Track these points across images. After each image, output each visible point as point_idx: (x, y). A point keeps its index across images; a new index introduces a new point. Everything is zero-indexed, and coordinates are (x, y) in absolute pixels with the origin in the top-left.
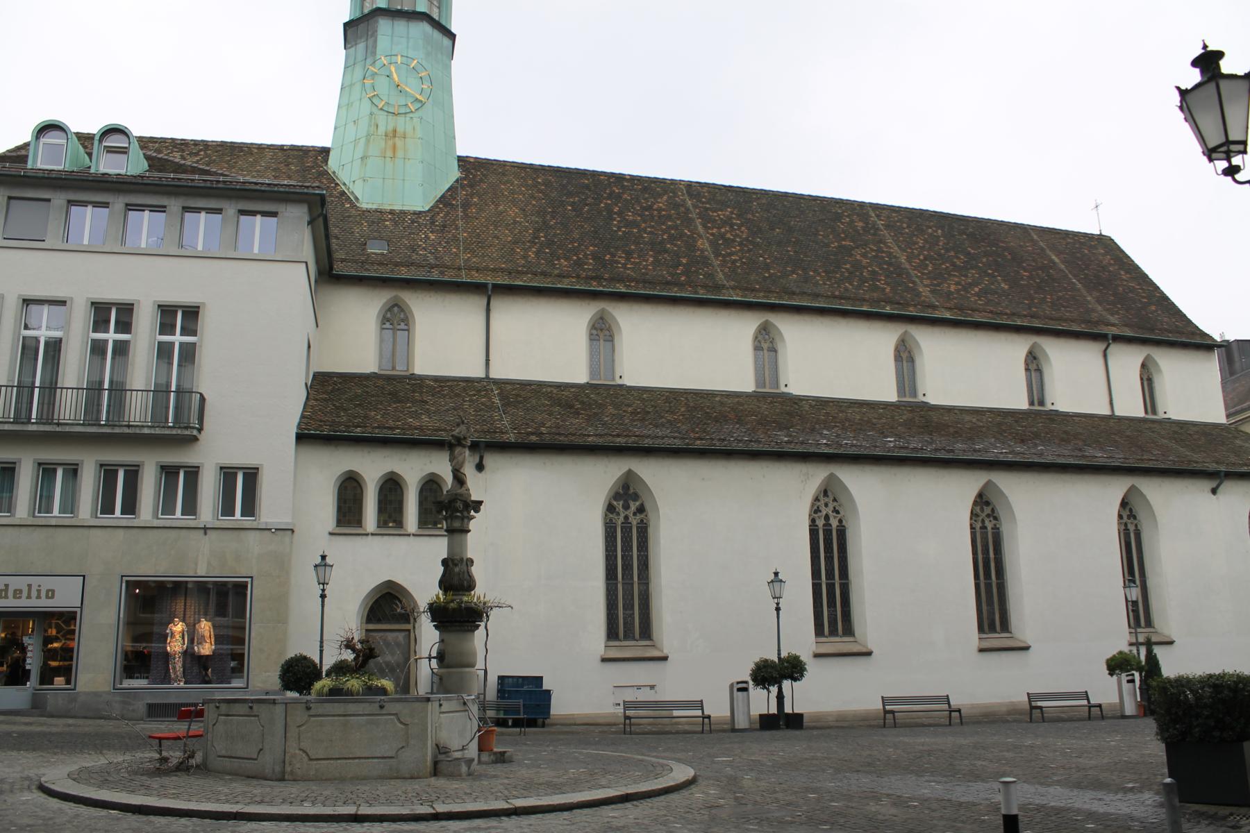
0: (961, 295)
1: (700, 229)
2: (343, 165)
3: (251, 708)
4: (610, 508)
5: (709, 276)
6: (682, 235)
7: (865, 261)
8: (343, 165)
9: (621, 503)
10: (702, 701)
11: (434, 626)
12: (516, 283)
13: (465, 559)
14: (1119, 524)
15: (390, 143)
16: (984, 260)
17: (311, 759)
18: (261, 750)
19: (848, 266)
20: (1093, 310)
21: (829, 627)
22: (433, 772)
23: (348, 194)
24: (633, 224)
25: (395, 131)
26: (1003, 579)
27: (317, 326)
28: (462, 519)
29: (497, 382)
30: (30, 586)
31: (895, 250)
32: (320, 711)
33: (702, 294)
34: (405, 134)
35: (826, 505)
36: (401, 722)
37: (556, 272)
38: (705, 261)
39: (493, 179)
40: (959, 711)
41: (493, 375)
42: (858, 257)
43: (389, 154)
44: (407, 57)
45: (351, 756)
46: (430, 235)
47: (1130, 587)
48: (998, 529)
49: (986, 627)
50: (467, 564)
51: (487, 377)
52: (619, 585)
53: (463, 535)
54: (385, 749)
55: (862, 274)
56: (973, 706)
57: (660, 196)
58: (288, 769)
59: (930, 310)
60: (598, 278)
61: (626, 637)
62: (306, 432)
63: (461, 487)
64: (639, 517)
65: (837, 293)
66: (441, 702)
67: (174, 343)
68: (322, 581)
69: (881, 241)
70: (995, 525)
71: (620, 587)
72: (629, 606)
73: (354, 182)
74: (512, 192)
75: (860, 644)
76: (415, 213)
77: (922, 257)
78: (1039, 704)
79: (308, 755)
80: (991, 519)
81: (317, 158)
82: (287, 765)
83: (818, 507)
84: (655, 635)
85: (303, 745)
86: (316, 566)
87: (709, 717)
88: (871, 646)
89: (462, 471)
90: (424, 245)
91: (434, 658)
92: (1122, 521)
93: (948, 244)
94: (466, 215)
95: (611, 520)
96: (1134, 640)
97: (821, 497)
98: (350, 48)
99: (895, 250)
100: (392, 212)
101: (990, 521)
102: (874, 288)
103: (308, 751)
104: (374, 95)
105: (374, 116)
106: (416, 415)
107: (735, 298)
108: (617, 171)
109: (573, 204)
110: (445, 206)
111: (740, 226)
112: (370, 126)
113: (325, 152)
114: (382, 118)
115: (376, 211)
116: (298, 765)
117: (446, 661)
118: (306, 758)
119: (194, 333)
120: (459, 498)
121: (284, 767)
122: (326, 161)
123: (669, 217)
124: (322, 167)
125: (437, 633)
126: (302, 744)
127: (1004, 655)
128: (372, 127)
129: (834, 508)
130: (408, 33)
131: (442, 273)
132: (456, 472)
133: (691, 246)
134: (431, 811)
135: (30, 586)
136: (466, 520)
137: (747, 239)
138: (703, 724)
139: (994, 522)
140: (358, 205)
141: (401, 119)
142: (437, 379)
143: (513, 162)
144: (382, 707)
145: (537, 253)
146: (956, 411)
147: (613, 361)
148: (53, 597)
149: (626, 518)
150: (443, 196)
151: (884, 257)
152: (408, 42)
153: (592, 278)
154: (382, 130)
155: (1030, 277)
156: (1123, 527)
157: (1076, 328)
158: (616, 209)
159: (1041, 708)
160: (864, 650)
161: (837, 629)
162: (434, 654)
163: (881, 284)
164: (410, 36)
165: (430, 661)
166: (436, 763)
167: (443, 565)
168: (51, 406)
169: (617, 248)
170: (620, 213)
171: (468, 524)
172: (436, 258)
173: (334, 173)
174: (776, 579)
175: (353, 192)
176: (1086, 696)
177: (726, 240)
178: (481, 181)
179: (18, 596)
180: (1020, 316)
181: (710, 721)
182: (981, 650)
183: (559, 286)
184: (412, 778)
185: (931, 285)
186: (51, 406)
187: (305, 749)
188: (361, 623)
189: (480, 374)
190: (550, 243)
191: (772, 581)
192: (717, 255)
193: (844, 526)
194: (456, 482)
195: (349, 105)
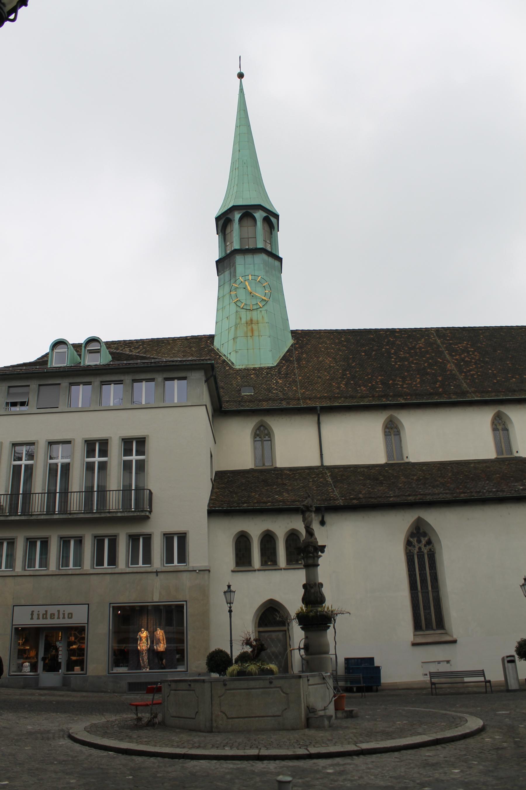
1: (448, 357)
3: (190, 685)
4: (408, 543)
8: (223, 344)
9: (415, 539)
10: (483, 671)
11: (301, 628)
12: (334, 405)
13: (317, 583)
15: (249, 327)
17: (228, 718)
18: (197, 712)
25: (251, 320)
28: (314, 558)
30: (59, 611)
33: (454, 399)
34: (258, 321)
36: (284, 692)
37: (359, 395)
43: (250, 334)
46: (279, 380)
50: (319, 587)
58: (215, 725)
60: (386, 396)
63: (311, 537)
64: (428, 547)
68: (229, 601)
72: (427, 607)
73: (230, 353)
79: (226, 715)
86: (225, 592)
87: (489, 682)
91: (302, 649)
95: (410, 551)
98: (221, 275)
100: (254, 369)
107: (476, 399)
112: (236, 319)
113: (211, 337)
114: (243, 314)
115: (245, 369)
124: (210, 347)
128: (238, 319)
131: (288, 403)
135: (59, 611)
136: (316, 559)
137: (479, 360)
141: (254, 313)
142: (291, 469)
144: (271, 683)
145: (346, 385)
148: (71, 618)
149: (420, 548)
152: (254, 267)
154: (244, 321)
158: (393, 351)
162: (302, 646)
165: (300, 651)
166: (308, 719)
171: (318, 561)
172: (284, 394)
178: (307, 344)
179: (52, 617)
183: (362, 403)
189: (315, 462)
192: (461, 372)
195: (223, 308)
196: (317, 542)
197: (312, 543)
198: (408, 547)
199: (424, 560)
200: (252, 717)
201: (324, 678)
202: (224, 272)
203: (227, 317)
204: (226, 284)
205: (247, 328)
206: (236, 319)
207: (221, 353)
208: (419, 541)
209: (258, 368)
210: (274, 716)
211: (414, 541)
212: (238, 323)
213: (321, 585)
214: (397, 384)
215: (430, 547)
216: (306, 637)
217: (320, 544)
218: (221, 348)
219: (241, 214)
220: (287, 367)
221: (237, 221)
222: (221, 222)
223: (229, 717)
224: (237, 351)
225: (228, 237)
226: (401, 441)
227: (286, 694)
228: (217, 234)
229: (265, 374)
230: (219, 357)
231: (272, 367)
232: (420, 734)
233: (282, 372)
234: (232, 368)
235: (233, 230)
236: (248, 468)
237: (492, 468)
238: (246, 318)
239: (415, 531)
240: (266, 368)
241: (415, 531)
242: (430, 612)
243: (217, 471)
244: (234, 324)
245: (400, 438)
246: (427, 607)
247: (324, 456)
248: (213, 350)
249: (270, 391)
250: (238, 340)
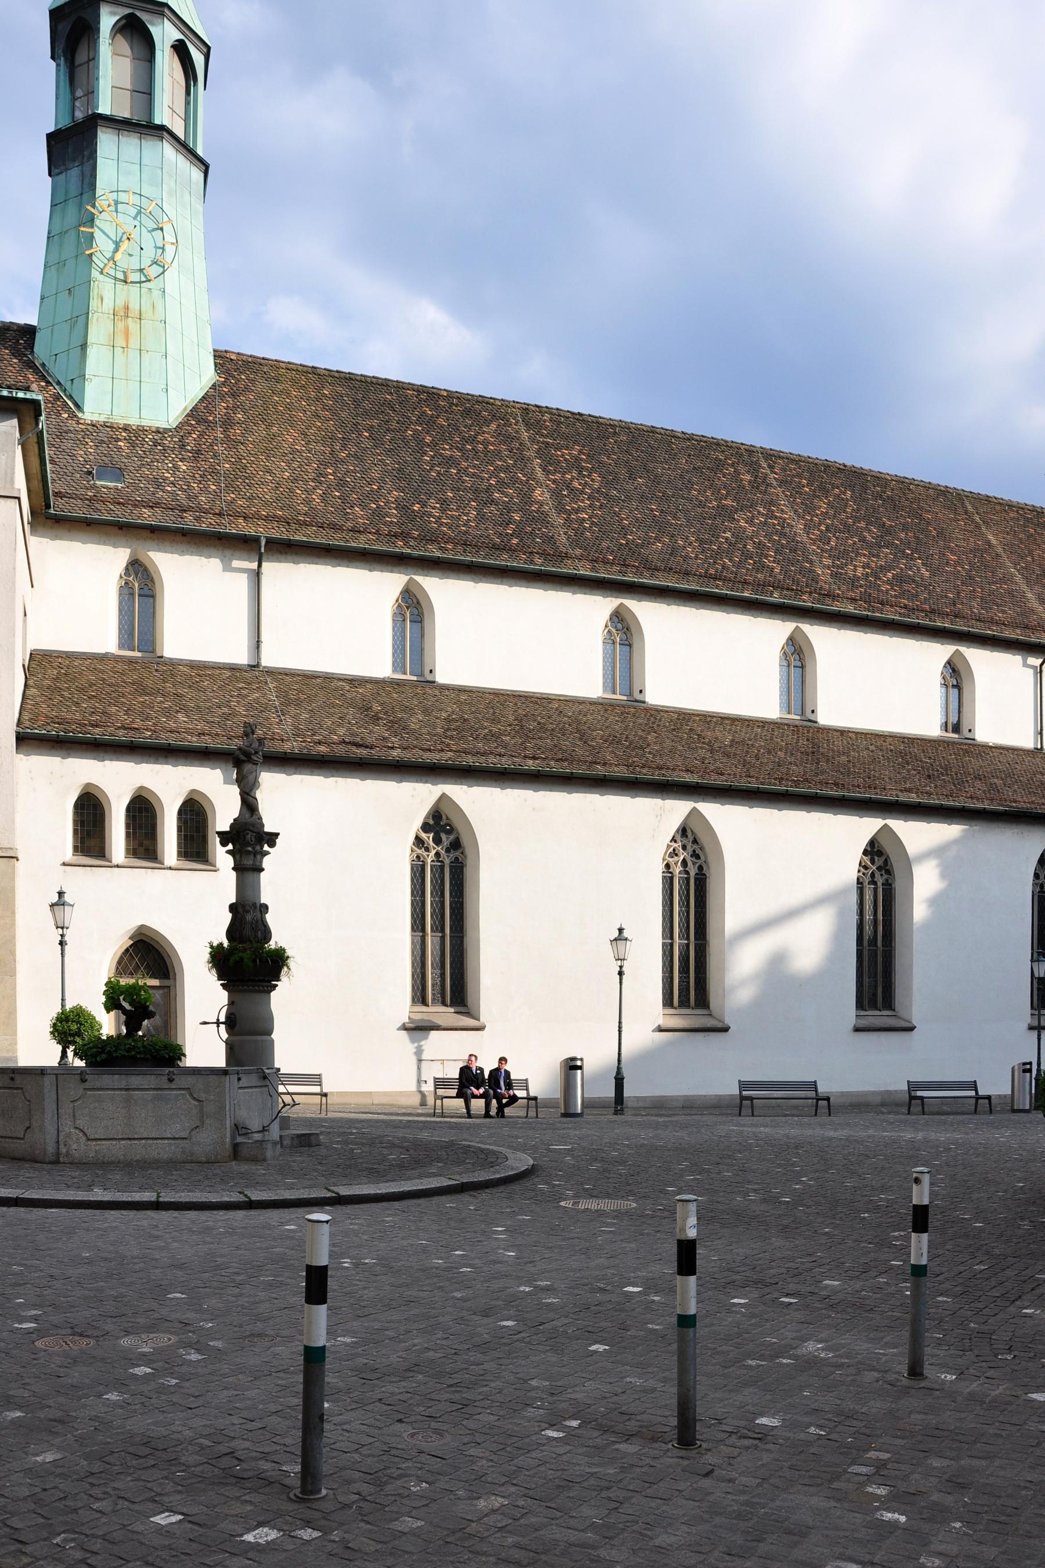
0: (870, 581)
1: (539, 473)
3: (12, 1079)
5: (550, 540)
6: (515, 480)
7: (750, 530)
9: (431, 835)
10: (526, 1080)
11: (221, 985)
12: (297, 538)
13: (258, 905)
14: (1034, 885)
16: (903, 535)
17: (89, 1140)
18: (28, 1128)
19: (728, 535)
20: (1033, 611)
21: (679, 997)
22: (232, 1155)
24: (450, 461)
25: (127, 308)
26: (891, 946)
27: (32, 586)
28: (255, 854)
29: (271, 672)
31: (789, 515)
32: (98, 1084)
33: (538, 564)
35: (684, 848)
36: (195, 1099)
37: (349, 524)
38: (543, 519)
39: (261, 385)
40: (828, 1099)
41: (268, 660)
42: (742, 523)
43: (120, 341)
45: (136, 1136)
46: (180, 463)
47: (1038, 961)
48: (891, 885)
49: (866, 1002)
50: (261, 911)
51: (255, 666)
53: (256, 874)
54: (176, 1128)
55: (745, 546)
56: (843, 1094)
57: (487, 423)
58: (63, 1150)
59: (829, 601)
60: (404, 536)
62: (29, 731)
63: (252, 816)
64: (453, 854)
65: (712, 571)
66: (240, 1076)
69: (772, 503)
70: (887, 880)
73: (72, 380)
74: (289, 407)
75: (714, 1018)
76: (157, 431)
77: (823, 528)
78: (919, 1094)
79: (85, 1134)
80: (883, 872)
82: (62, 1146)
83: (674, 850)
84: (470, 1000)
85: (79, 1123)
86: (52, 905)
87: (535, 1099)
88: (728, 1021)
89: (252, 795)
90: (172, 479)
91: (222, 1023)
92: (1037, 881)
93: (858, 510)
94: (227, 437)
95: (418, 857)
96: (1036, 1024)
97: (678, 838)
98: (58, 174)
99: (789, 515)
100: (126, 428)
101: (882, 875)
102: (760, 567)
103: (85, 1130)
106: (167, 713)
107: (581, 572)
108: (429, 384)
110: (198, 422)
111: (591, 472)
115: (105, 425)
116: (74, 1146)
117: (237, 1028)
118: (84, 1138)
120: (251, 828)
121: (58, 1148)
122: (31, 346)
123: (498, 454)
124: (26, 355)
125: (225, 994)
126: (78, 1122)
127: (883, 1035)
129: (694, 851)
131: (198, 519)
132: (245, 796)
133: (527, 497)
134: (241, 1198)
136: (259, 857)
137: (598, 491)
138: (528, 1107)
139: (885, 876)
140: (80, 415)
142: (193, 665)
143: (289, 363)
144: (171, 1080)
145: (324, 498)
146: (850, 734)
147: (422, 649)
149: (437, 854)
150: (195, 409)
151: (774, 525)
155: (958, 563)
156: (1038, 889)
157: (1009, 634)
158: (428, 439)
159: (922, 1098)
160: (720, 1025)
161: (689, 999)
162: (222, 1019)
163: (769, 561)
165: (218, 1026)
166: (236, 1146)
167: (230, 912)
169: (429, 495)
170: (434, 445)
171: (261, 862)
172: (189, 497)
173: (43, 365)
174: (620, 937)
175: (70, 395)
176: (974, 1086)
177: (572, 490)
178: (246, 389)
180: (943, 615)
181: (536, 1103)
182: (857, 1030)
183: (353, 544)
184: (208, 1162)
185: (833, 566)
187: (81, 1128)
189: (241, 657)
190: (341, 483)
191: (616, 939)
192: (560, 509)
193: (705, 875)
194: (245, 810)
195: (61, 264)
196: (263, 826)
197: (253, 825)
200: (134, 1139)
201: (265, 1077)
207: (51, 376)
208: (437, 841)
209: (134, 428)
210: (174, 1139)
213: (265, 908)
214: (430, 515)
216: (231, 1003)
217: (268, 829)
219: (117, 18)
220: (202, 435)
221: (107, 35)
222: (65, 27)
223: (90, 1138)
225: (80, 73)
226: (423, 636)
227: (198, 1101)
228: (53, 58)
229: (151, 443)
231: (166, 430)
232: (434, 1175)
234: (76, 416)
235: (94, 59)
237: (589, 717)
239: (431, 822)
240: (154, 429)
241: (431, 822)
243: (35, 650)
245: (422, 628)
249: (159, 486)
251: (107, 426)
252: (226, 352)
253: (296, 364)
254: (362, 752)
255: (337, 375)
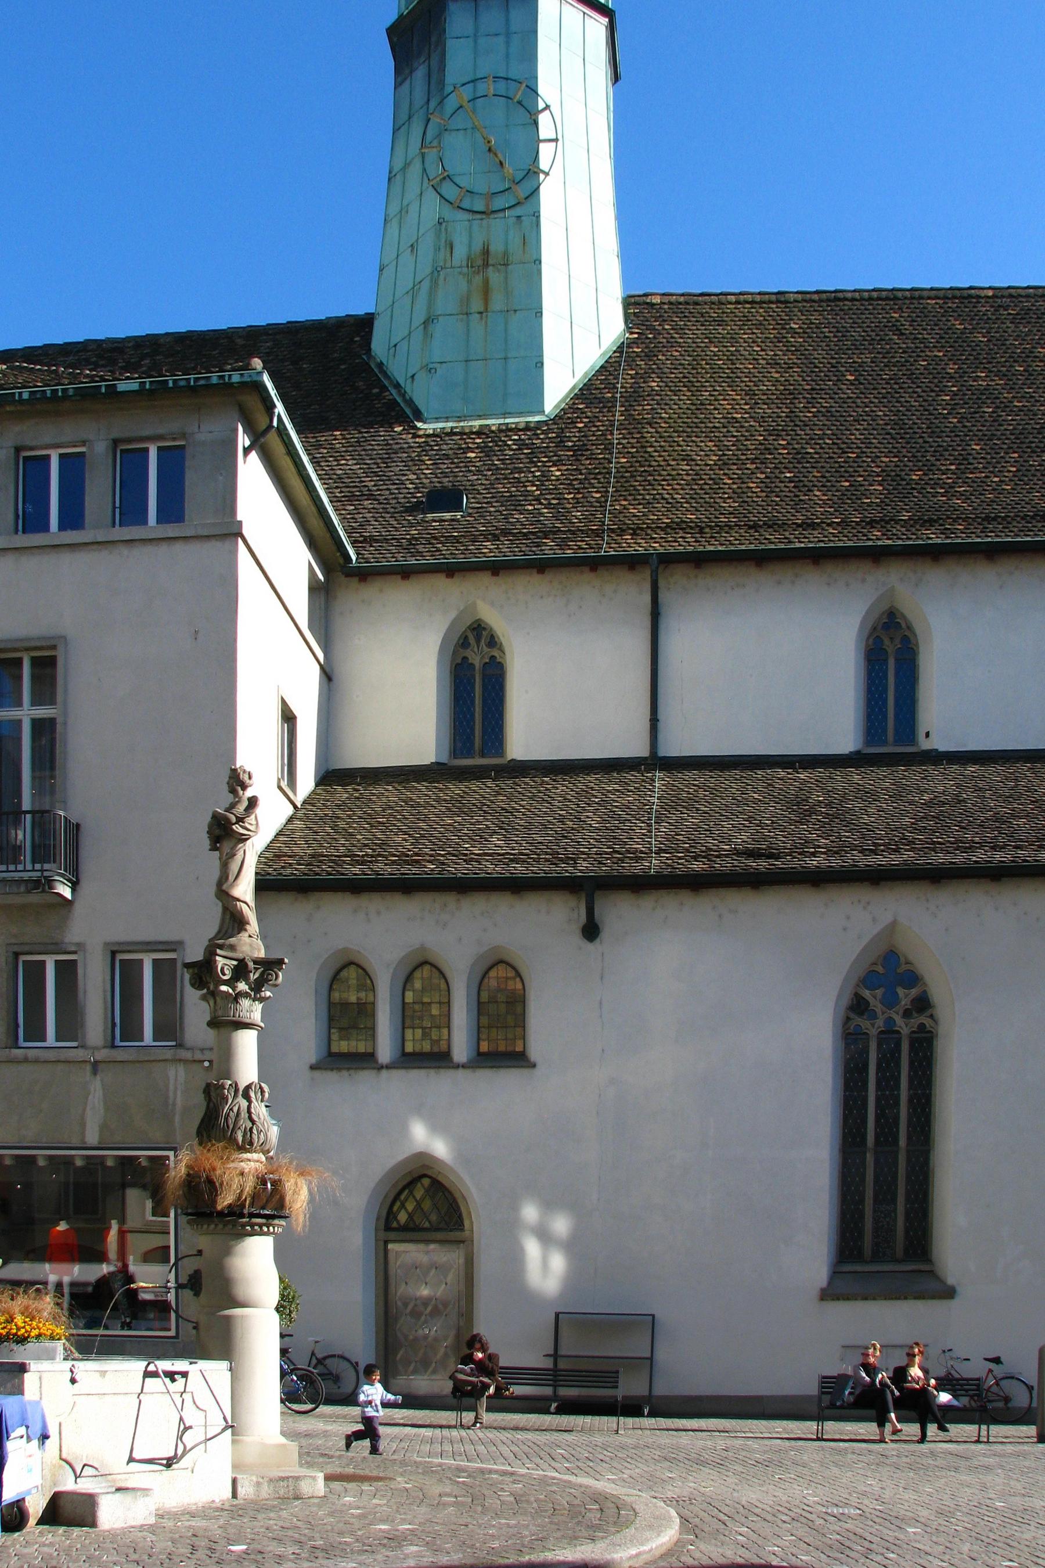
2: (395, 346)
4: (858, 1006)
8: (395, 346)
15: (478, 280)
23: (402, 405)
25: (486, 252)
34: (506, 254)
43: (477, 305)
44: (507, 79)
52: (868, 1155)
60: (884, 523)
61: (877, 1256)
67: (20, 721)
71: (870, 1158)
72: (885, 1194)
73: (413, 377)
81: (352, 340)
104: (444, 178)
105: (444, 225)
109: (857, 369)
112: (438, 249)
113: (364, 324)
114: (460, 226)
119: (52, 702)
128: (442, 250)
130: (507, 20)
131: (563, 545)
141: (497, 224)
145: (768, 487)
152: (508, 43)
153: (872, 524)
154: (460, 252)
164: (513, 28)
168: (145, 947)
178: (671, 343)
186: (145, 947)
188: (376, 1229)
198: (852, 1015)
199: (900, 1057)
202: (411, 73)
203: (412, 245)
204: (415, 119)
205: (469, 282)
206: (435, 250)
208: (890, 1001)
211: (873, 997)
212: (441, 264)
215: (923, 1019)
218: (391, 357)
224: (431, 366)
230: (381, 392)
233: (569, 440)
236: (427, 762)
238: (470, 246)
242: (895, 1210)
244: (428, 270)
246: (885, 1194)
247: (661, 725)
248: (366, 368)
250: (437, 329)
251: (455, 434)
252: (646, 295)
253: (752, 294)
254: (762, 865)
255: (816, 297)
